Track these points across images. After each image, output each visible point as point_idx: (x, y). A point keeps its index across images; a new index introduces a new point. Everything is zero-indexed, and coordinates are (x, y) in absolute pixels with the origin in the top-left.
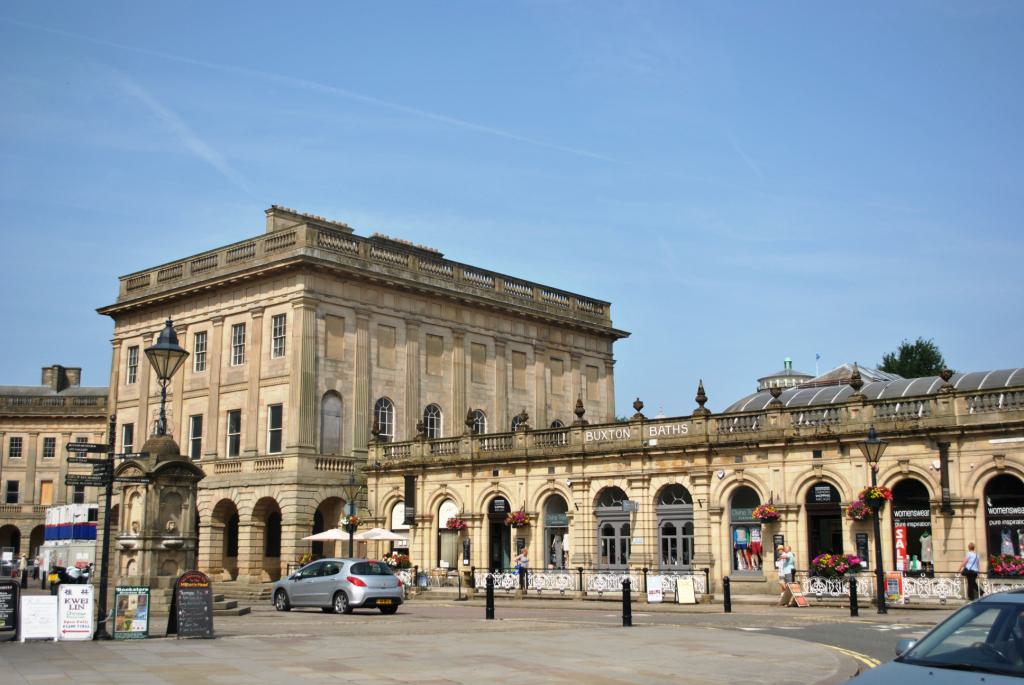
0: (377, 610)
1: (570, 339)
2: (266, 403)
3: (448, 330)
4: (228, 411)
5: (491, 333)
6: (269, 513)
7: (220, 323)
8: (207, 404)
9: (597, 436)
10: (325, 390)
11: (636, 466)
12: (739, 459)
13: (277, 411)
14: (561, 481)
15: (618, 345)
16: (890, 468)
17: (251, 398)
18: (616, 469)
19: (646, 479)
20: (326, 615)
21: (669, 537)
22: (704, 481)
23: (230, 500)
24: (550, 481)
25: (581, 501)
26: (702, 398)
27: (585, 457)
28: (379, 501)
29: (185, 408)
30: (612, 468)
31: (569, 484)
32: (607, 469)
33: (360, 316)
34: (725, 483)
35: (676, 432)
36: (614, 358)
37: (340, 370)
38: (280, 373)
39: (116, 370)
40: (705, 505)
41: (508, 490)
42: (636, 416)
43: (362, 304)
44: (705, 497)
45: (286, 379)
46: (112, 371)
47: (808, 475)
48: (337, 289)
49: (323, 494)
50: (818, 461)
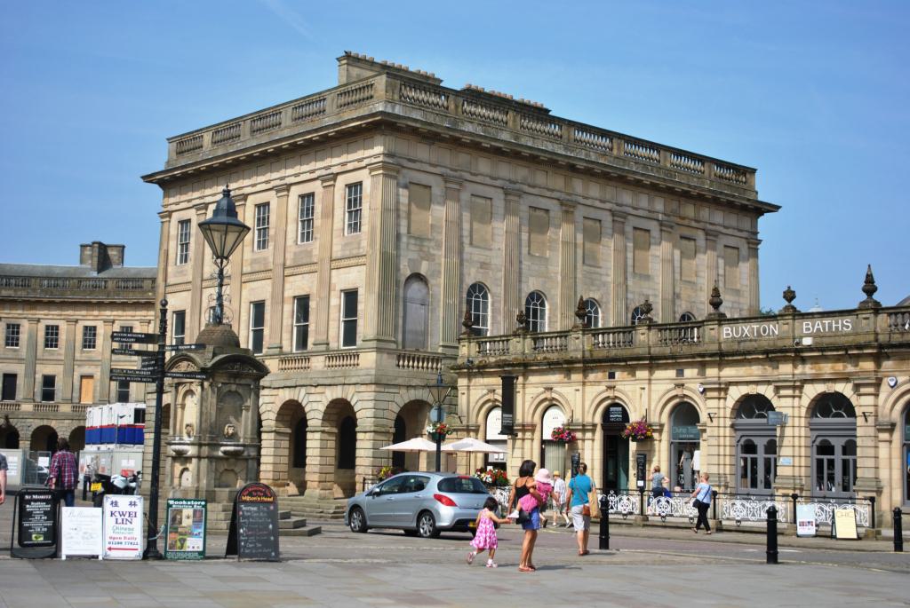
2: (338, 288)
3: (555, 202)
4: (294, 297)
5: (608, 206)
6: (342, 418)
8: (270, 289)
10: (408, 273)
11: (786, 369)
13: (351, 297)
15: (764, 222)
17: (321, 282)
18: (760, 373)
21: (825, 458)
22: (871, 390)
25: (716, 411)
28: (472, 405)
30: (755, 371)
31: (701, 390)
32: (749, 372)
35: (837, 328)
36: (759, 237)
37: (425, 249)
38: (355, 252)
39: (165, 247)
41: (627, 396)
42: (786, 308)
43: (452, 170)
46: (160, 249)
48: (423, 152)
49: (406, 396)
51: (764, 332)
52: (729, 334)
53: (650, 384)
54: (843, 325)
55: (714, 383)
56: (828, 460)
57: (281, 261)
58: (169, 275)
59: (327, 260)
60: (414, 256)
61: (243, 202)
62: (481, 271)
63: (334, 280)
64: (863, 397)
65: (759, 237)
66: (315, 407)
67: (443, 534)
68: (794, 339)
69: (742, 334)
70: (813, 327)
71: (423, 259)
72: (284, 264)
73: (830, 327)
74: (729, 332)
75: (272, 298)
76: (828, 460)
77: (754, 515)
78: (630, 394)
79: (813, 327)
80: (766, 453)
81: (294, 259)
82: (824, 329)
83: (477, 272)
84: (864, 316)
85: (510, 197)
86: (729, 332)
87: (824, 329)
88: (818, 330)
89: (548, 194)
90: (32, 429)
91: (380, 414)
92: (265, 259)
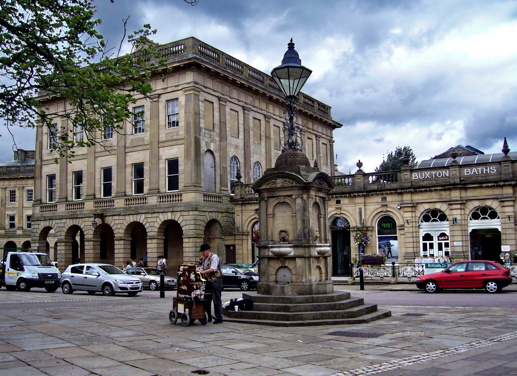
0: (44, 289)
2: (164, 158)
3: (262, 116)
4: (132, 164)
5: (282, 120)
6: (172, 232)
7: (157, 99)
8: (115, 160)
9: (422, 176)
10: (206, 149)
11: (456, 195)
13: (173, 165)
14: (392, 206)
15: (336, 132)
17: (152, 155)
18: (438, 197)
19: (463, 203)
20: (9, 292)
21: (428, 242)
22: (511, 203)
23: (75, 225)
24: (337, 208)
25: (411, 218)
27: (416, 188)
28: (244, 221)
29: (97, 163)
30: (434, 196)
31: (399, 207)
32: (431, 197)
33: (221, 102)
35: (487, 172)
36: (334, 139)
37: (212, 137)
38: (175, 137)
39: (40, 139)
41: (349, 212)
42: (358, 171)
43: (222, 94)
44: (512, 214)
45: (180, 142)
46: (37, 140)
48: (209, 83)
49: (209, 217)
50: (339, 206)
51: (439, 175)
52: (416, 177)
53: (242, 213)
54: (490, 170)
55: (410, 204)
56: (430, 244)
57: (123, 144)
58: (43, 155)
59: (156, 143)
60: (207, 140)
61: (157, 99)
62: (235, 150)
63: (161, 154)
64: (506, 208)
65: (334, 139)
66: (153, 224)
67: (97, 293)
68: (241, 195)
69: (425, 177)
70: (471, 171)
71: (211, 141)
72: (125, 146)
73: (482, 171)
74: (469, 171)
75: (150, 161)
76: (430, 244)
77: (372, 274)
78: (351, 212)
79: (471, 171)
80: (423, 240)
81: (132, 143)
82: (478, 172)
83: (234, 150)
84: (505, 164)
85: (246, 112)
86: (469, 171)
87: (478, 172)
88: (475, 173)
89: (260, 111)
90: (22, 243)
91: (198, 227)
92: (143, 138)
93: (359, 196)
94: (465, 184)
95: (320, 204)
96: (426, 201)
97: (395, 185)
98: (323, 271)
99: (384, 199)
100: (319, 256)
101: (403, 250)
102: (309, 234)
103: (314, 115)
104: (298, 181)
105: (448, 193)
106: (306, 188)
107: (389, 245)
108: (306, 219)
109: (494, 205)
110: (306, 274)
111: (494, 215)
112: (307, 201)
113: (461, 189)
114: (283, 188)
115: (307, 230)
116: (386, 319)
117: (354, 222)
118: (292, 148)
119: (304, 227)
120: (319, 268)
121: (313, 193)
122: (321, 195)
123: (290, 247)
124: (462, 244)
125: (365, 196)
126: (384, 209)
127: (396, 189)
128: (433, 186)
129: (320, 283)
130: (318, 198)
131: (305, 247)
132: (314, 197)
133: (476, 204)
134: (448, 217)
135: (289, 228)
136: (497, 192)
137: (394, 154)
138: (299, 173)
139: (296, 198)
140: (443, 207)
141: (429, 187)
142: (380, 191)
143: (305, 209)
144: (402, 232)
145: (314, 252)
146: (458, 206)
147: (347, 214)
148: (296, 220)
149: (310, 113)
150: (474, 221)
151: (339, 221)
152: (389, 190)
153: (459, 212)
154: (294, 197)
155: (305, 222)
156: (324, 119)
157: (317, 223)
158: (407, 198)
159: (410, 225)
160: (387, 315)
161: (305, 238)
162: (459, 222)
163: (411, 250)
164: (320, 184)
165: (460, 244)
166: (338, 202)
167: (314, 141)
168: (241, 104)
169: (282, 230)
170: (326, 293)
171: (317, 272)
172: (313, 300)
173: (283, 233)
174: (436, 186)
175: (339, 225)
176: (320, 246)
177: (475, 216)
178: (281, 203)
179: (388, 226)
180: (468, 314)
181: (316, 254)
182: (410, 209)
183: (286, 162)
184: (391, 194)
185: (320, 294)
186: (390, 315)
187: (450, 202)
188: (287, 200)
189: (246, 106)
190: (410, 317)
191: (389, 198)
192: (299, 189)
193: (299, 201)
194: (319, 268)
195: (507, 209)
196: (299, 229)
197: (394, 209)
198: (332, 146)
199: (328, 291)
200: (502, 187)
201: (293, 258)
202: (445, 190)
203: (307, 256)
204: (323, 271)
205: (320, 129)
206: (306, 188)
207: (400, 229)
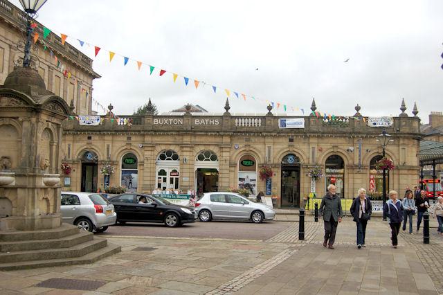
1: (78, 74)
11: (187, 139)
12: (248, 140)
15: (95, 82)
16: (328, 149)
21: (162, 177)
26: (227, 108)
27: (156, 132)
30: (170, 140)
34: (238, 152)
40: (228, 162)
41: (98, 147)
47: (285, 150)
50: (90, 141)
73: (208, 123)
78: (100, 147)
93: (108, 134)
94: (195, 132)
95: (52, 129)
96: (164, 143)
97: (139, 127)
98: (52, 203)
99: (129, 139)
100: (46, 187)
101: (142, 182)
102: (35, 163)
103: (78, 64)
104: (27, 102)
105: (181, 137)
106: (36, 110)
107: (130, 178)
108: (33, 145)
109: (215, 150)
110: (28, 207)
111: (214, 158)
112: (35, 125)
113: (191, 135)
114: (8, 108)
115: (34, 158)
116: (115, 257)
117: (102, 156)
118: (26, 67)
119: (30, 154)
120: (47, 200)
121: (44, 117)
122: (55, 121)
123: (12, 176)
124: (34, 182)
125: (113, 135)
126: (128, 147)
127: (139, 131)
128: (170, 131)
129: (47, 216)
130: (50, 124)
131: (30, 176)
132: (45, 122)
133: (202, 148)
134: (180, 157)
135: (13, 154)
136: (218, 140)
137: (142, 109)
138: (29, 93)
139: (22, 121)
140: (176, 149)
141: (167, 131)
142: (126, 131)
143: (32, 134)
144: (142, 167)
145: (41, 182)
146: (188, 149)
147: (96, 149)
148: (22, 146)
149: (73, 61)
150: (199, 161)
151: (89, 154)
152: (134, 131)
153: (188, 153)
154: (20, 119)
155: (32, 148)
156: (86, 69)
157: (49, 152)
158: (148, 139)
159: (149, 162)
160: (117, 251)
161: (30, 166)
162: (188, 162)
163: (148, 183)
164: (54, 108)
165: (188, 179)
166: (90, 138)
167: (76, 86)
168: (8, 42)
169: (5, 155)
170: (51, 228)
171: (45, 203)
172: (32, 237)
173: (6, 160)
174: (172, 131)
175: (89, 158)
176: (49, 176)
177: (201, 158)
178: (7, 125)
179: (130, 161)
180: (196, 247)
181: (43, 185)
182: (150, 149)
183: (16, 79)
184: (135, 135)
185: (44, 229)
186: (121, 251)
187: (182, 146)
188: (13, 122)
189: (13, 45)
190: (140, 252)
191: (133, 138)
192: (28, 111)
193: (26, 124)
194: (47, 200)
195: (224, 154)
196: (23, 156)
197: (137, 147)
198: (91, 93)
199: (53, 226)
200: (222, 136)
201: (15, 189)
202: (179, 135)
203: (32, 187)
204: (52, 203)
205: (82, 77)
206: (36, 110)
207: (140, 165)
